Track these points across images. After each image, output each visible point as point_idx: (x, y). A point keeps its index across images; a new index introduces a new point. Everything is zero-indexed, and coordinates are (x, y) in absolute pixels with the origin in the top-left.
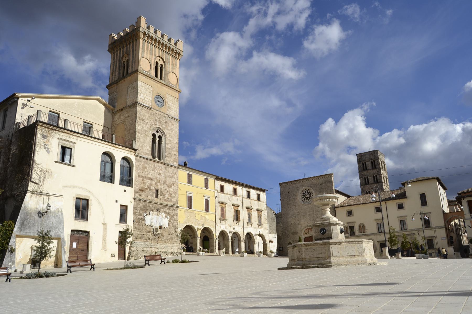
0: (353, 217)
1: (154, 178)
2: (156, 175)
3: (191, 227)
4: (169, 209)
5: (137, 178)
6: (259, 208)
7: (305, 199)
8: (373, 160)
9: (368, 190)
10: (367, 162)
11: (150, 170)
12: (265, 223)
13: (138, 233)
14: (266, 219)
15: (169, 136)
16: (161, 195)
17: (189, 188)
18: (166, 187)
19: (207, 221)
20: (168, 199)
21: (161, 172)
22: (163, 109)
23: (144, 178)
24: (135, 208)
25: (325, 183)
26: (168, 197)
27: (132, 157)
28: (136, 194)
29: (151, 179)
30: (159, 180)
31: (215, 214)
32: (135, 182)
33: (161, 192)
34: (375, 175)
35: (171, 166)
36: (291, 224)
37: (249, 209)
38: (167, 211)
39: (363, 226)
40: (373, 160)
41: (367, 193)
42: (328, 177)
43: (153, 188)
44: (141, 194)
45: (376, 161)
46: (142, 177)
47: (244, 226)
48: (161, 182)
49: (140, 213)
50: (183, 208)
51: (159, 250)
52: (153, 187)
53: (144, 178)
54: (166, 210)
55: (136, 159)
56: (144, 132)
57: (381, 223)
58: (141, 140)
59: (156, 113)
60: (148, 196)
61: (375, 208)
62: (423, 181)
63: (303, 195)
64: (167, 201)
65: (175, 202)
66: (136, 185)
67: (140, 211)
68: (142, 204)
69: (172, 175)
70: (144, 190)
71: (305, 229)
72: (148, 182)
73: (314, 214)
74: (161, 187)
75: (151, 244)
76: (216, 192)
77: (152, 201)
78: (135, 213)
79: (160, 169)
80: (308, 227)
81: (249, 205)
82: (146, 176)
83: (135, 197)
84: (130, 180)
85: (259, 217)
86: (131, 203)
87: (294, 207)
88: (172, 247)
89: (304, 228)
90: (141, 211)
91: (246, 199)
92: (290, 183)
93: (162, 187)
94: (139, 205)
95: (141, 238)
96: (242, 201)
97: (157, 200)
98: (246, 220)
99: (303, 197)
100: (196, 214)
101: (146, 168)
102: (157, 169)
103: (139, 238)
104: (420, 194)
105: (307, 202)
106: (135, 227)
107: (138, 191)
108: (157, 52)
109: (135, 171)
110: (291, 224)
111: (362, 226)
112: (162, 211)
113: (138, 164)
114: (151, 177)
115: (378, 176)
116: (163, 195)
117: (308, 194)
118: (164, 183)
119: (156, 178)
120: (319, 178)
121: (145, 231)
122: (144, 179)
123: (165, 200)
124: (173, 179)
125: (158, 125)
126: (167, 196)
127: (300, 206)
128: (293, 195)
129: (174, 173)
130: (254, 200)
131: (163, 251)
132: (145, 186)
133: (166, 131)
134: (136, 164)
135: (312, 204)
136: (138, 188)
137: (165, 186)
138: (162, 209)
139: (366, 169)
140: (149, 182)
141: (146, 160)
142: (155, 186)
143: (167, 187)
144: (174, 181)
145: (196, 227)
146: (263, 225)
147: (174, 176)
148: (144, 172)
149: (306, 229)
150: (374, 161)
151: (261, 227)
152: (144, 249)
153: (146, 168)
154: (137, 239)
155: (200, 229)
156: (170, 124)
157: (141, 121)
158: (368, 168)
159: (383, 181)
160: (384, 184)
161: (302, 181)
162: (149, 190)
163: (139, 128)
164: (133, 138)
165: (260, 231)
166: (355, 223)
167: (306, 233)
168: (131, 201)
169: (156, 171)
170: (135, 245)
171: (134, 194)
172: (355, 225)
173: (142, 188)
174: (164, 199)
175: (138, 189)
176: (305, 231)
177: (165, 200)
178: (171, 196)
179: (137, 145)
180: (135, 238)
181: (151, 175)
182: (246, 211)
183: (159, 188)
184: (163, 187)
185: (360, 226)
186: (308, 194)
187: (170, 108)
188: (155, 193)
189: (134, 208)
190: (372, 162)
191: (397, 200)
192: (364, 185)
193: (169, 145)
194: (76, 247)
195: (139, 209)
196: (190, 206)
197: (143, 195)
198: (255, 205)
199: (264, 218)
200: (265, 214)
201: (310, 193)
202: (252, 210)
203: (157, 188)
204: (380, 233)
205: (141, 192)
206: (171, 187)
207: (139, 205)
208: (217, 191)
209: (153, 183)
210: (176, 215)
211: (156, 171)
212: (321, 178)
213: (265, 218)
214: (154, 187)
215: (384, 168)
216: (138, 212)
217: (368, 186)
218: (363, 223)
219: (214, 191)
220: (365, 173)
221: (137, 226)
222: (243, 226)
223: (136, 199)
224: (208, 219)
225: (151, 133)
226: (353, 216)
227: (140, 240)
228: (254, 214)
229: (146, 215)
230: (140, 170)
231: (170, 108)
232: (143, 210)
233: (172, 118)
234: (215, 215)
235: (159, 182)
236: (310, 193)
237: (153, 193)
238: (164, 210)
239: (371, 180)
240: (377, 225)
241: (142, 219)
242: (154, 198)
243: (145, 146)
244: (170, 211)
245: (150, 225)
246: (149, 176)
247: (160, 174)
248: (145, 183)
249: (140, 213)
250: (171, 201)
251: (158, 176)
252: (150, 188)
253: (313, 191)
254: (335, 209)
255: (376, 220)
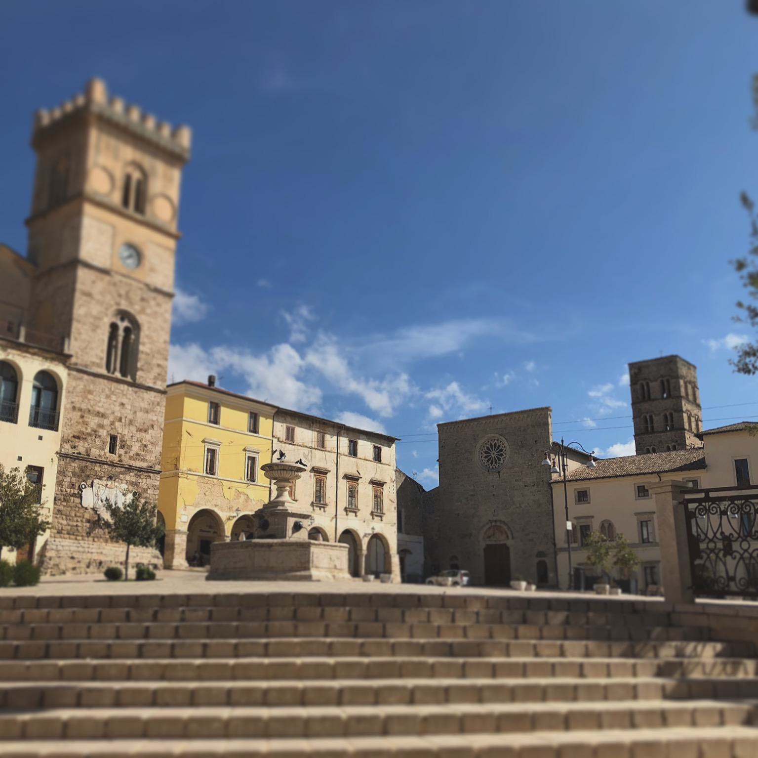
0: (588, 505)
1: (109, 412)
2: (112, 406)
3: (213, 513)
4: (139, 476)
5: (68, 413)
6: (378, 477)
7: (490, 462)
8: (665, 379)
9: (651, 445)
10: (652, 381)
11: (99, 396)
12: (389, 510)
13: (64, 522)
14: (392, 501)
15: (149, 328)
16: (122, 447)
17: (213, 433)
18: (135, 432)
19: (250, 503)
20: (138, 455)
21: (125, 401)
22: (139, 274)
23: (84, 412)
24: (61, 473)
25: (533, 426)
26: (138, 452)
27: (60, 371)
28: (65, 444)
29: (101, 415)
30: (118, 418)
31: (270, 488)
32: (63, 421)
33: (122, 441)
34: (668, 414)
35: (149, 389)
36: (458, 515)
37: (352, 479)
38: (134, 480)
39: (610, 525)
40: (665, 379)
41: (648, 452)
42: (539, 414)
43: (103, 433)
44: (76, 444)
45: (672, 381)
46: (80, 410)
47: (338, 516)
48: (123, 420)
49: (71, 482)
50: (195, 473)
51: (109, 559)
52: (105, 431)
53: (83, 413)
54: (131, 477)
55: (69, 375)
56: (91, 320)
57: (648, 522)
58: (84, 336)
59: (121, 281)
60: (92, 449)
61: (637, 487)
62: (731, 432)
63: (486, 452)
64: (134, 460)
65: (153, 462)
66: (65, 426)
67: (71, 479)
68: (76, 465)
69: (149, 408)
70: (84, 437)
71: (488, 526)
72: (93, 422)
73: (507, 495)
74: (121, 429)
75: (91, 546)
76: (275, 440)
77: (101, 459)
78: (59, 483)
79: (124, 395)
80: (494, 524)
81: (352, 471)
82: (90, 408)
83: (63, 450)
84: (54, 417)
85: (376, 496)
86: (52, 462)
87: (467, 477)
88: (140, 554)
89: (484, 526)
90: (74, 479)
91: (346, 458)
92: (460, 425)
93: (126, 432)
94: (71, 466)
95: (71, 533)
96: (336, 462)
97: (112, 457)
98: (344, 502)
99: (486, 457)
100: (225, 488)
101: (90, 392)
102: (115, 395)
103: (65, 532)
104: (735, 460)
105: (500, 465)
106: (59, 511)
107: (70, 438)
108: (128, 153)
109: (67, 398)
110: (458, 515)
111: (606, 525)
112: (122, 480)
113: (74, 384)
114: (102, 410)
115: (675, 415)
116: (126, 447)
117: (497, 449)
118: (131, 423)
119: (113, 413)
120: (522, 417)
121: (79, 520)
122: (85, 415)
123: (130, 457)
124: (152, 416)
125: (124, 305)
126: (136, 448)
127: (478, 476)
128: (464, 452)
129: (156, 403)
130: (367, 460)
131: (117, 560)
132: (86, 429)
133: (141, 319)
134: (68, 383)
135: (504, 474)
136: (69, 432)
137: (133, 429)
138: (121, 476)
139: (650, 399)
140: (96, 421)
141: (91, 378)
142: (109, 430)
143: (137, 431)
144: (155, 418)
145: (223, 515)
146: (384, 514)
147: (155, 409)
148: (86, 401)
149: (490, 528)
150: (668, 381)
151: (380, 518)
152: (75, 555)
153: (90, 392)
154: (62, 535)
155: (231, 518)
156: (152, 303)
157: (84, 298)
158: (652, 397)
159: (686, 426)
160: (687, 435)
161: (484, 422)
162: (94, 436)
163: (80, 310)
164: (65, 333)
165: (375, 527)
166: (593, 520)
167: (489, 537)
168: (52, 460)
169: (114, 398)
170: (54, 547)
171: (61, 445)
172: (592, 523)
173: (80, 432)
174: (128, 457)
175: (71, 435)
176: (485, 533)
177: (131, 458)
178: (144, 449)
179: (73, 347)
180: (56, 531)
181: (103, 406)
182: (344, 485)
183: (118, 433)
184: (128, 432)
185: (602, 526)
186: (497, 449)
187: (152, 270)
188: (109, 444)
189: (59, 472)
190: (662, 383)
191: (684, 472)
192: (644, 434)
193: (148, 346)
194: (710, 496)
195: (70, 474)
196: (211, 469)
197: (80, 447)
198: (368, 471)
199: (388, 500)
200: (392, 491)
201: (500, 448)
202: (360, 481)
203: (113, 433)
204: (646, 544)
205: (77, 440)
206: (145, 432)
207: (71, 466)
208: (278, 439)
209: (106, 422)
210: (154, 489)
211: (114, 398)
212: (526, 416)
213: (390, 500)
214: (108, 431)
215: (691, 398)
216: (68, 479)
217: (650, 435)
218: (609, 521)
219: (272, 438)
220: (645, 406)
221: (61, 508)
222: (336, 515)
223: (62, 456)
224: (252, 498)
225: (107, 321)
226: (589, 503)
227: (67, 536)
228: (365, 492)
229: (83, 486)
230: (77, 396)
231: (152, 270)
232: (79, 476)
233: (157, 291)
234: (270, 491)
235: (120, 420)
236: (500, 448)
237: (104, 443)
238: (128, 478)
239: (658, 421)
240: (640, 525)
241: (74, 495)
242: (105, 453)
243: (92, 349)
244: (140, 481)
245: (92, 507)
246: (97, 409)
247: (122, 404)
248: (86, 424)
249: (71, 482)
250: (144, 460)
251: (117, 408)
252: (97, 433)
253: (506, 444)
254: (551, 485)
255: (637, 514)
